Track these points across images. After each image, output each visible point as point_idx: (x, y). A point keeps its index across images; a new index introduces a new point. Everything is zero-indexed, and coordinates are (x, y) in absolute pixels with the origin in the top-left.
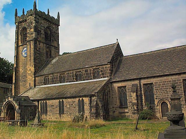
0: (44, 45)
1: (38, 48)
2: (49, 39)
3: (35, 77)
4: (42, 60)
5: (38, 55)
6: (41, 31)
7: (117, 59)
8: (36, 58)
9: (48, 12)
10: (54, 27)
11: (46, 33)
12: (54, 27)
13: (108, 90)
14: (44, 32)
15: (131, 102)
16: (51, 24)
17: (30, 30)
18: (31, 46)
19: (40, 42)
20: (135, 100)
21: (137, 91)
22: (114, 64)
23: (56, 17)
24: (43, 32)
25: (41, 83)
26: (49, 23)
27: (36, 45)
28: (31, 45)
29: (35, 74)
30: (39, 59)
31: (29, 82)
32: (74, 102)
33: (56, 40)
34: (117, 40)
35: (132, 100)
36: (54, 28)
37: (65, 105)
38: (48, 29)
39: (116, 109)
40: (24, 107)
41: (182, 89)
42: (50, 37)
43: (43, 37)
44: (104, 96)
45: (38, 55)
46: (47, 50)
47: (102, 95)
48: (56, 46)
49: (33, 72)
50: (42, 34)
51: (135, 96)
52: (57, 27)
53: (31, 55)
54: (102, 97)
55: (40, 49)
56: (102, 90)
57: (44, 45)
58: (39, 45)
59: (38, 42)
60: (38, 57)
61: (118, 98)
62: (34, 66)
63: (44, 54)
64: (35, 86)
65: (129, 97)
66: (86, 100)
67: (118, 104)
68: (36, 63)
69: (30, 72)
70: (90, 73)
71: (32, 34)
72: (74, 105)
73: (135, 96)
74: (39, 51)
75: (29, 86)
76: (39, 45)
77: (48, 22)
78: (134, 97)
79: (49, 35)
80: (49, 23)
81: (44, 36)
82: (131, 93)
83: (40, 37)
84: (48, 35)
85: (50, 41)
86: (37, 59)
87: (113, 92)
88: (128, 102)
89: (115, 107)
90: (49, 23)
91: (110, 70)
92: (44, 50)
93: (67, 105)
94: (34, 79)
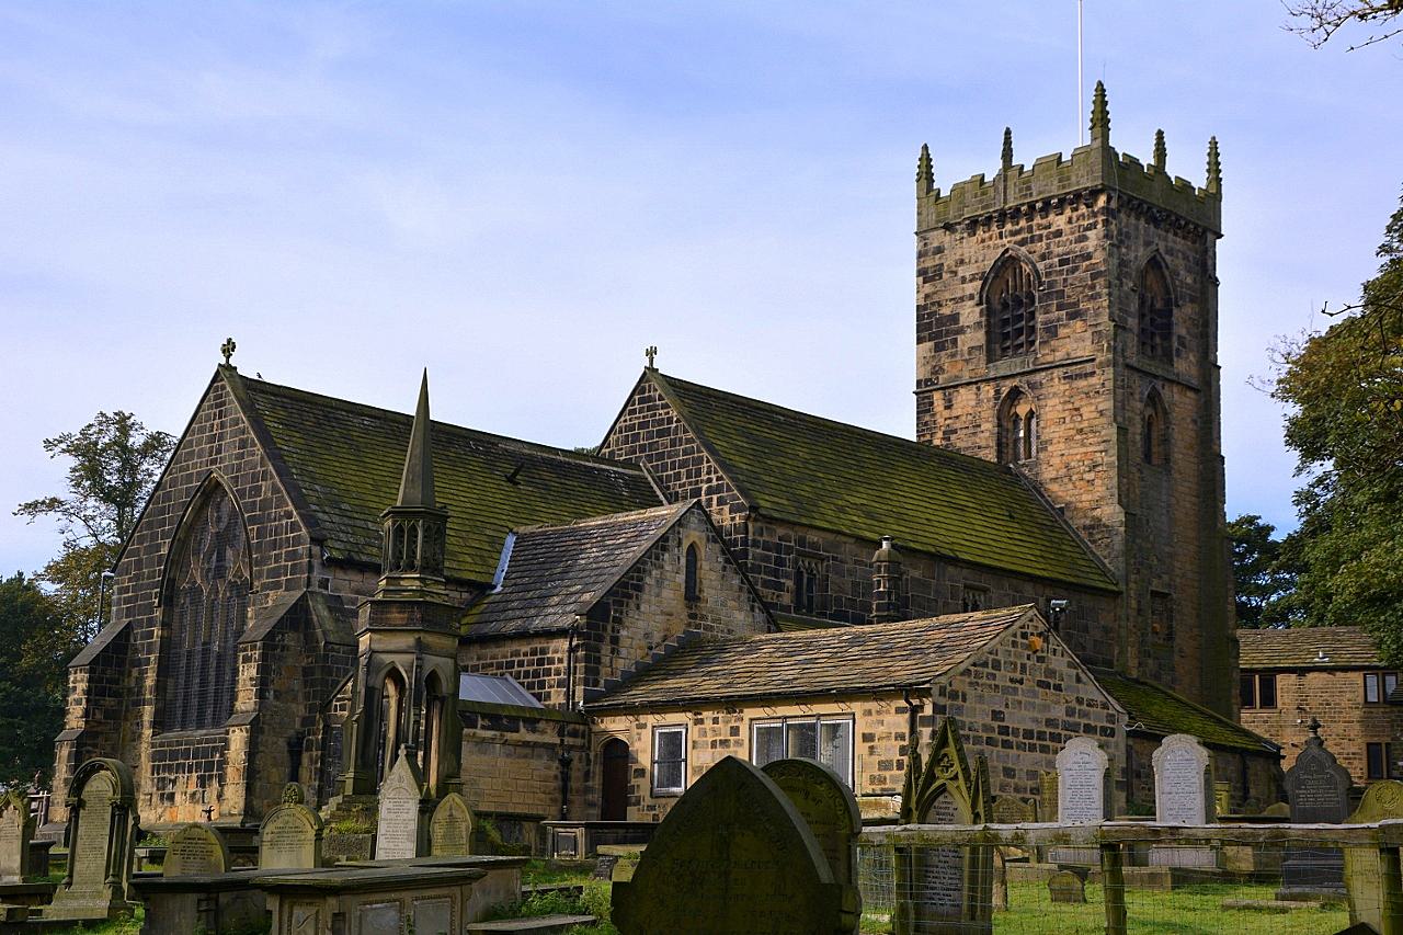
6: (955, 318)
9: (1007, 154)
10: (1059, 221)
14: (978, 309)
24: (970, 314)
34: (651, 353)
36: (1059, 233)
77: (1009, 226)
81: (979, 337)
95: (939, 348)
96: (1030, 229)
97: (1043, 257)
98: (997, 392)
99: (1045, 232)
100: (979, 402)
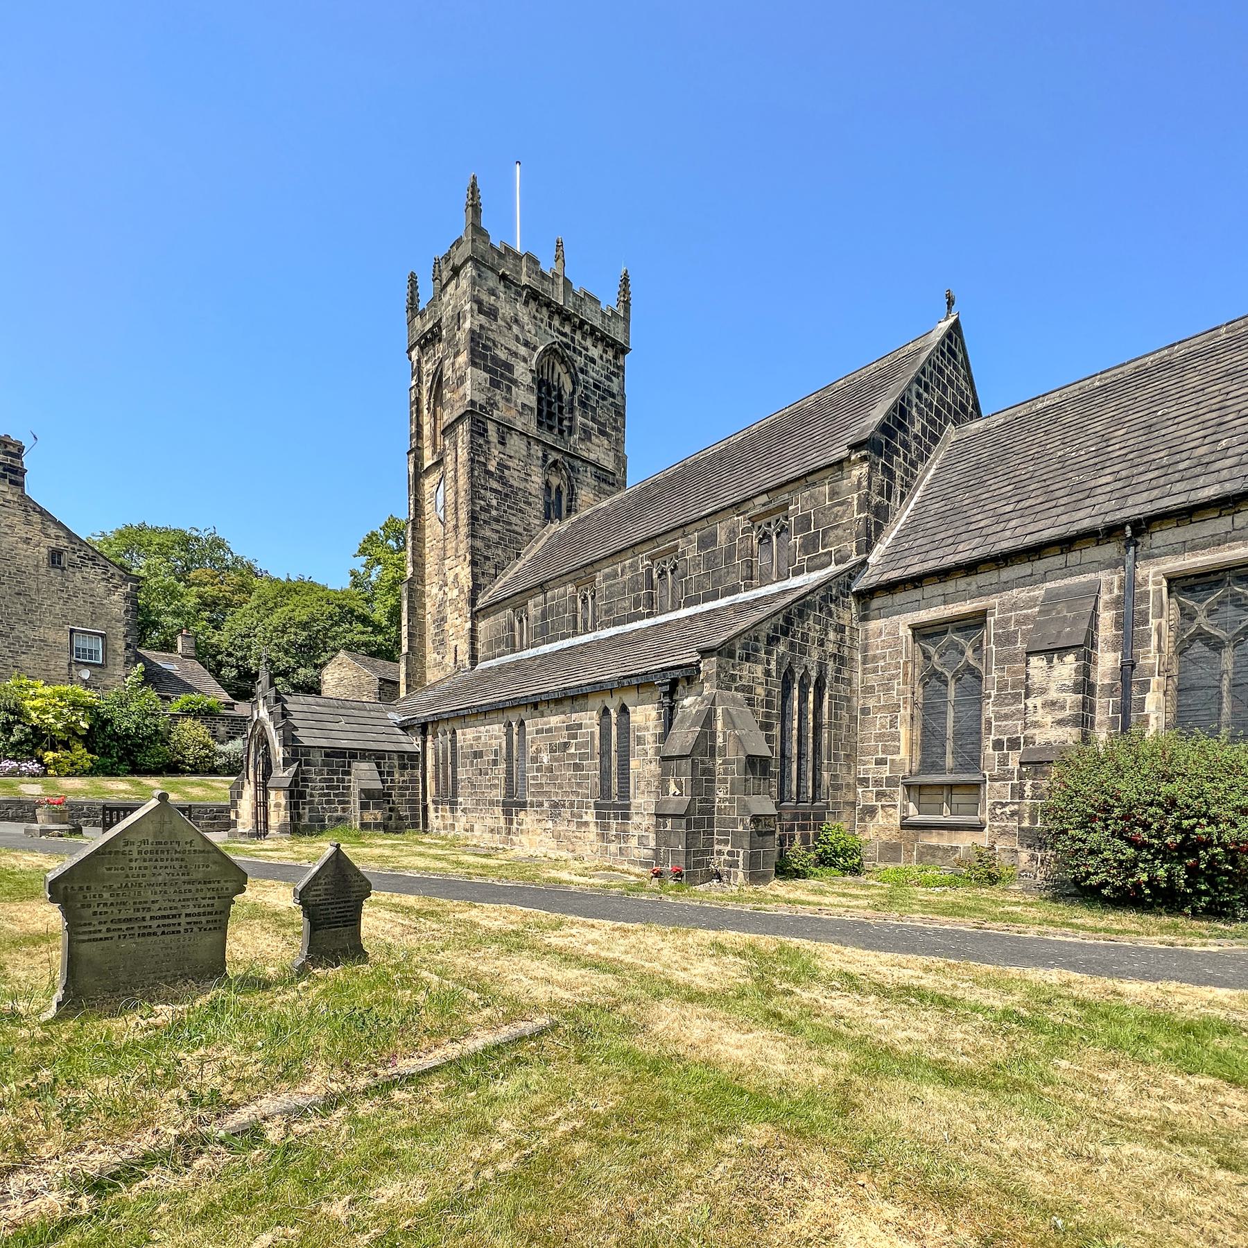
0: (529, 449)
1: (494, 463)
2: (566, 423)
3: (475, 616)
4: (520, 530)
5: (494, 502)
6: (510, 368)
7: (935, 439)
8: (484, 516)
10: (595, 352)
11: (543, 386)
12: (595, 352)
13: (831, 648)
15: (1014, 744)
16: (578, 336)
17: (453, 364)
18: (459, 450)
19: (506, 429)
20: (1060, 723)
21: (1091, 641)
22: (906, 471)
23: (609, 300)
24: (522, 373)
25: (498, 642)
26: (567, 329)
27: (481, 441)
28: (460, 444)
29: (473, 602)
30: (498, 521)
31: (454, 643)
32: (574, 729)
33: (603, 433)
35: (1036, 725)
36: (593, 361)
37: (531, 751)
38: (563, 362)
39: (880, 795)
40: (327, 755)
41: (782, 830)
42: (572, 410)
43: (524, 405)
44: (786, 694)
45: (494, 502)
46: (555, 481)
47: (767, 673)
48: (609, 463)
49: (466, 590)
50: (514, 382)
51: (1062, 689)
52: (616, 357)
53: (460, 501)
54: (769, 694)
55: (508, 468)
56: (772, 640)
57: (529, 449)
58: (502, 443)
59: (491, 427)
60: (494, 513)
61: (905, 713)
62: (469, 558)
63: (531, 500)
64: (474, 658)
65: (1000, 701)
66: (645, 716)
67: (903, 754)
68: (479, 544)
69: (456, 592)
70: (730, 554)
71: (461, 380)
72: (572, 750)
73: (1062, 689)
74: (502, 479)
75: (452, 665)
76: (503, 444)
78: (1053, 695)
79: (566, 397)
80: (562, 324)
81: (532, 400)
82: (1034, 661)
83: (508, 400)
84: (560, 398)
85: (571, 430)
86: (485, 522)
87: (875, 670)
88: (988, 743)
89: (877, 782)
90: (567, 329)
91: (865, 504)
92: (534, 478)
93: (538, 751)
94: (469, 625)
95: (495, 384)
96: (573, 340)
97: (582, 371)
98: (545, 456)
99: (584, 352)
100: (529, 455)
